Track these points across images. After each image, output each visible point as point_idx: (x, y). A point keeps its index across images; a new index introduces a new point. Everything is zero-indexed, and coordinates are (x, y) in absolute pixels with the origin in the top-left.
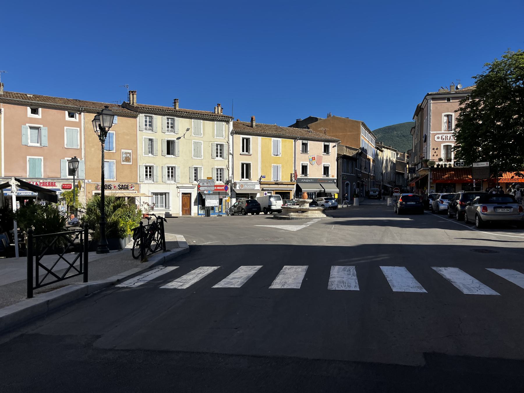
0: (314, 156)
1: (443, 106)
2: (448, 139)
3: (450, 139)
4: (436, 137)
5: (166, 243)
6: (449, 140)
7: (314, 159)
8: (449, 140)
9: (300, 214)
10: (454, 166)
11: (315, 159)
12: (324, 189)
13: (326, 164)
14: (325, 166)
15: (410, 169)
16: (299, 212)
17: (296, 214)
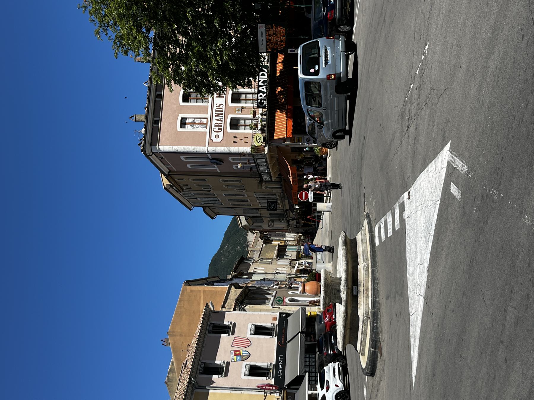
0: (233, 352)
1: (166, 130)
2: (221, 122)
3: (221, 119)
4: (215, 140)
5: (211, 375)
6: (222, 121)
7: (237, 353)
8: (222, 121)
9: (361, 288)
10: (264, 107)
11: (239, 351)
12: (298, 334)
13: (250, 329)
14: (253, 332)
15: (270, 208)
16: (355, 293)
17: (361, 299)
